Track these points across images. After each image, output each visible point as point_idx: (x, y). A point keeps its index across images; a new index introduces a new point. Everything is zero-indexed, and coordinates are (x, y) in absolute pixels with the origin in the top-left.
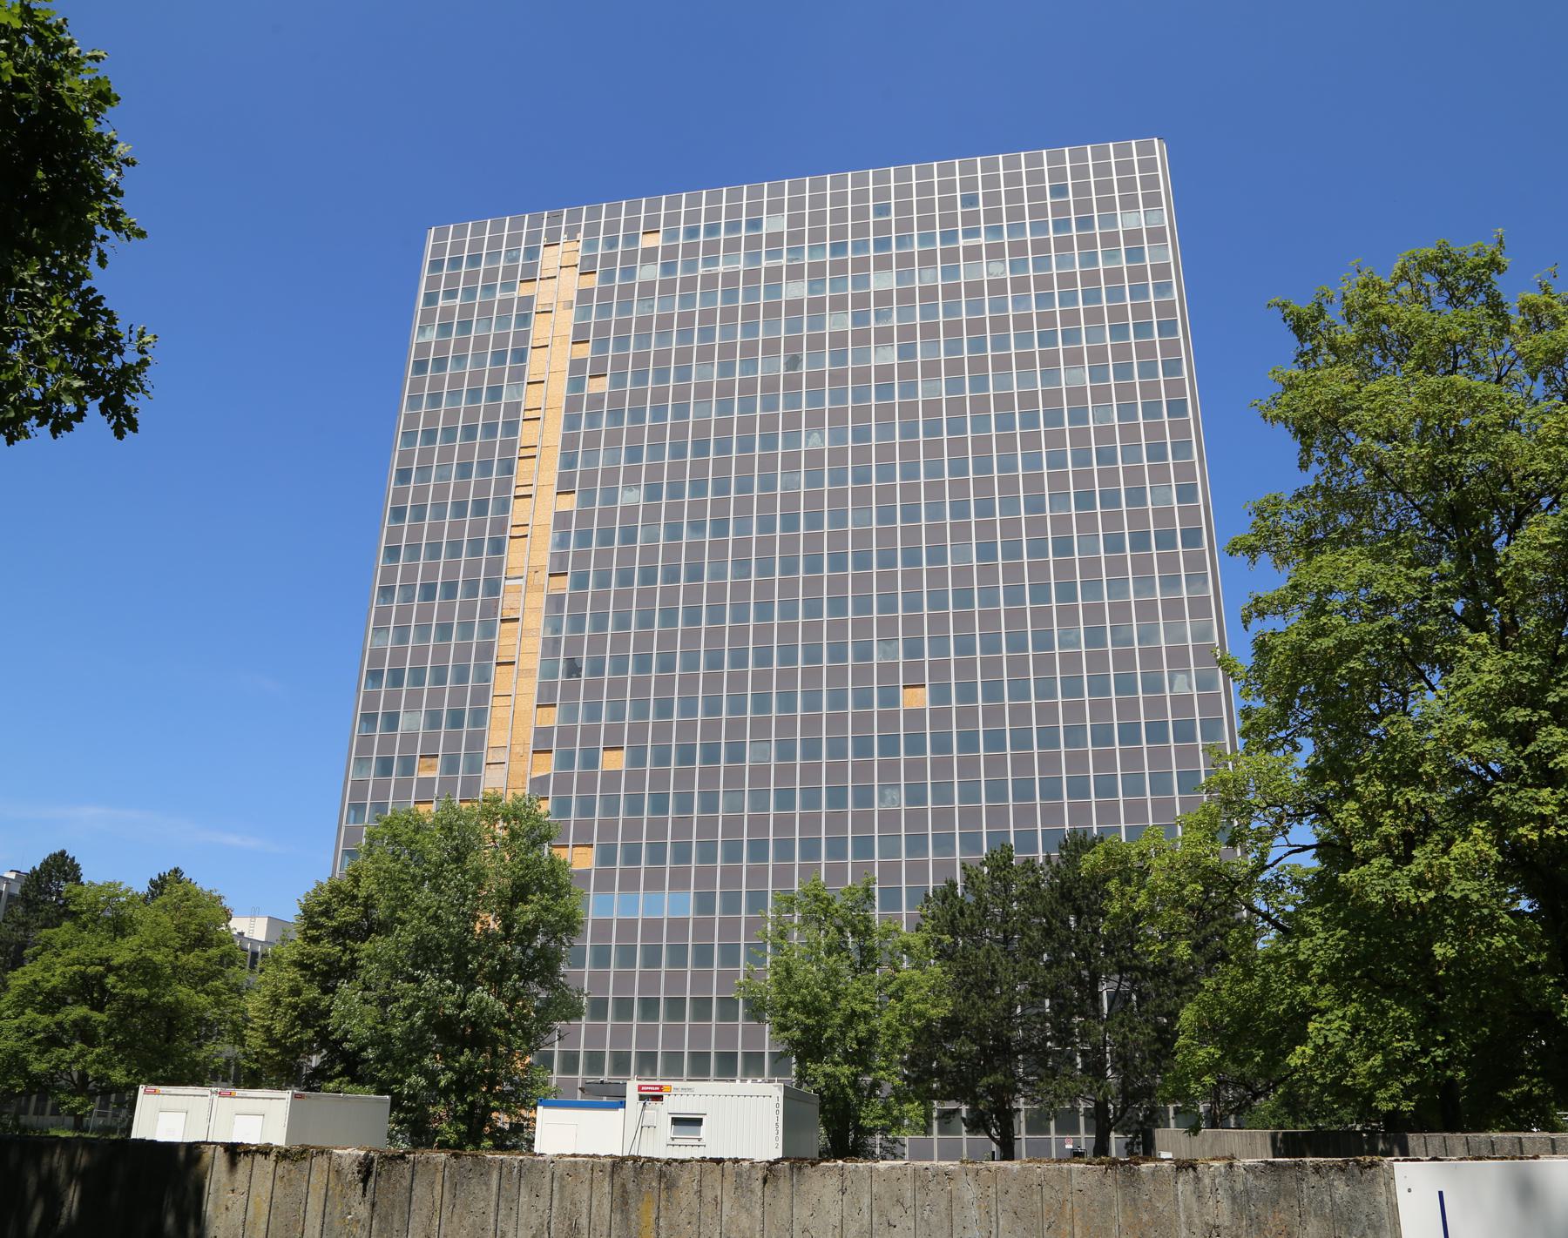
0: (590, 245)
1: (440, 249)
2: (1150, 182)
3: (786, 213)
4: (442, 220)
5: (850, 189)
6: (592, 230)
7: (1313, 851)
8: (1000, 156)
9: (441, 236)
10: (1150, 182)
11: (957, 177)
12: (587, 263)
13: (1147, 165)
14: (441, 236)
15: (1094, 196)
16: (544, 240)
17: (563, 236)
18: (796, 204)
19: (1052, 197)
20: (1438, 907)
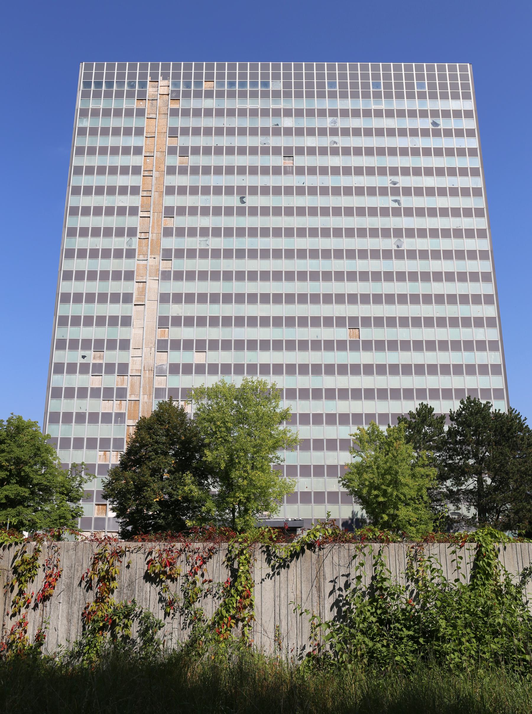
0: (176, 84)
1: (88, 76)
2: (465, 86)
3: (282, 80)
4: (89, 58)
5: (94, 71)
6: (176, 76)
7: (516, 581)
8: (182, 63)
9: (89, 68)
10: (465, 86)
11: (127, 71)
12: (174, 95)
13: (464, 77)
14: (89, 68)
15: (304, 90)
16: (149, 79)
17: (160, 78)
18: (287, 76)
19: (373, 88)
20: (502, 710)
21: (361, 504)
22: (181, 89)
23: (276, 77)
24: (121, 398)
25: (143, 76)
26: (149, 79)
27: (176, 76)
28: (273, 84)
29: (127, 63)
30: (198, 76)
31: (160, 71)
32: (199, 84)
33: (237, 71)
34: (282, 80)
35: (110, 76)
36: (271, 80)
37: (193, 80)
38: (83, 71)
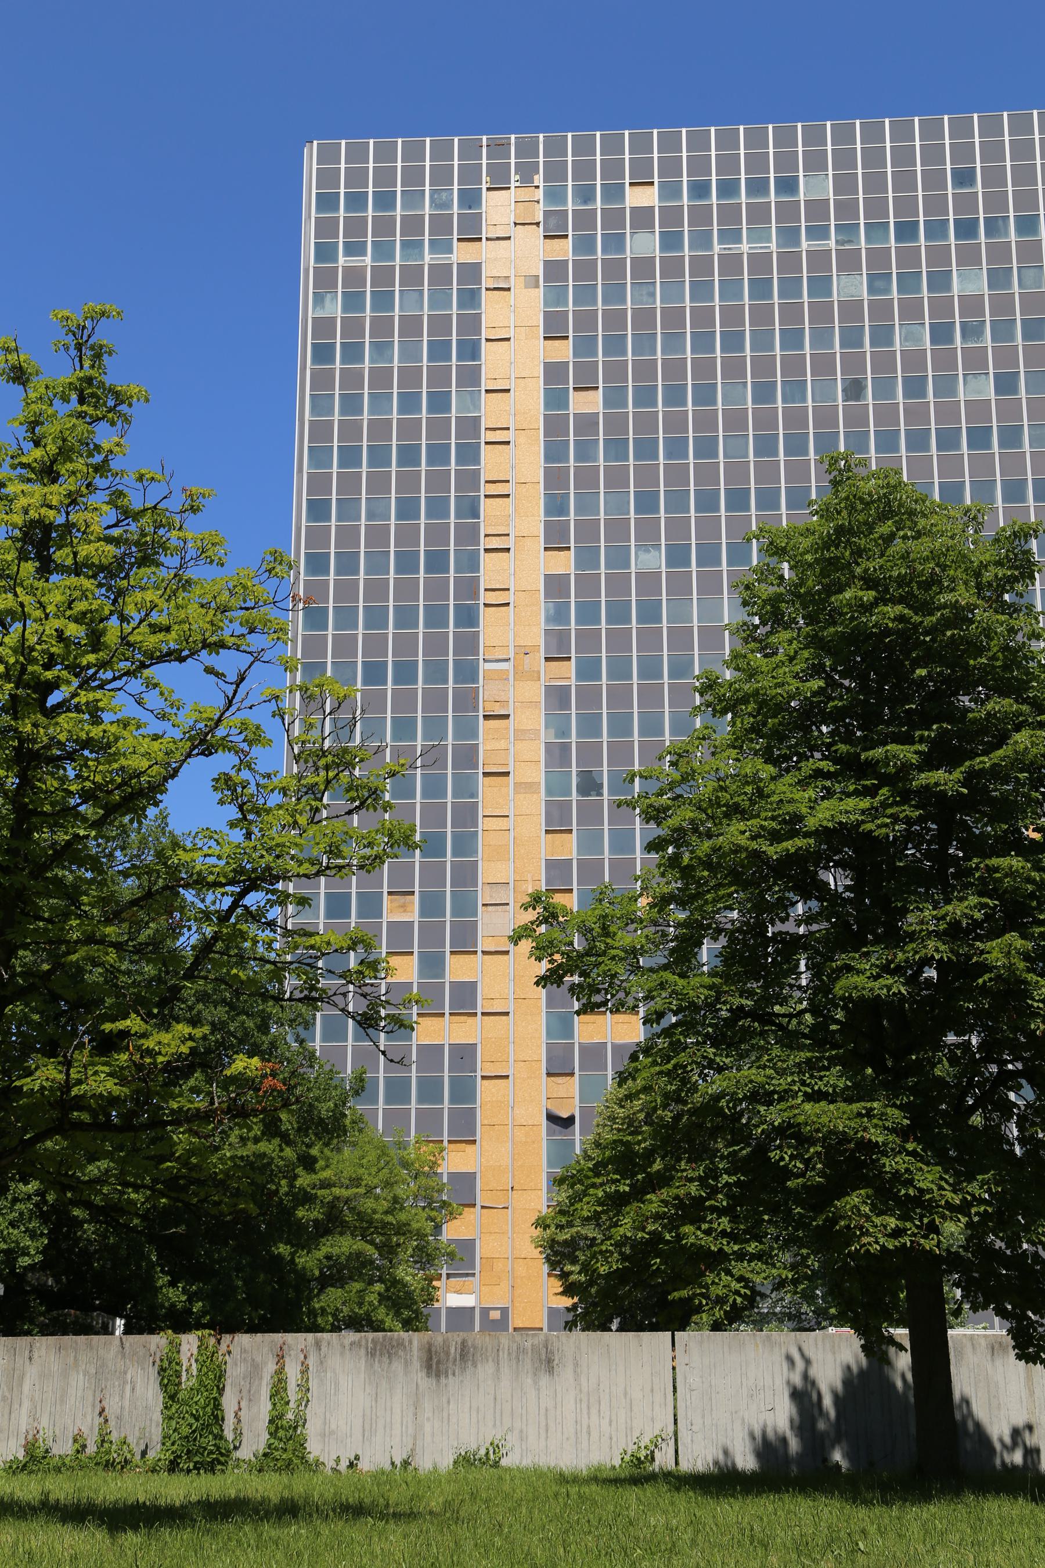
0: (554, 195)
1: (327, 178)
3: (830, 172)
8: (627, 132)
9: (328, 155)
12: (552, 222)
16: (485, 182)
21: (378, 1477)
22: (570, 207)
23: (815, 163)
24: (462, 1008)
25: (470, 174)
26: (485, 182)
27: (555, 172)
28: (806, 184)
29: (858, 122)
30: (612, 169)
31: (513, 161)
32: (614, 192)
33: (627, 156)
34: (830, 172)
35: (385, 176)
36: (801, 174)
37: (599, 182)
38: (315, 166)
